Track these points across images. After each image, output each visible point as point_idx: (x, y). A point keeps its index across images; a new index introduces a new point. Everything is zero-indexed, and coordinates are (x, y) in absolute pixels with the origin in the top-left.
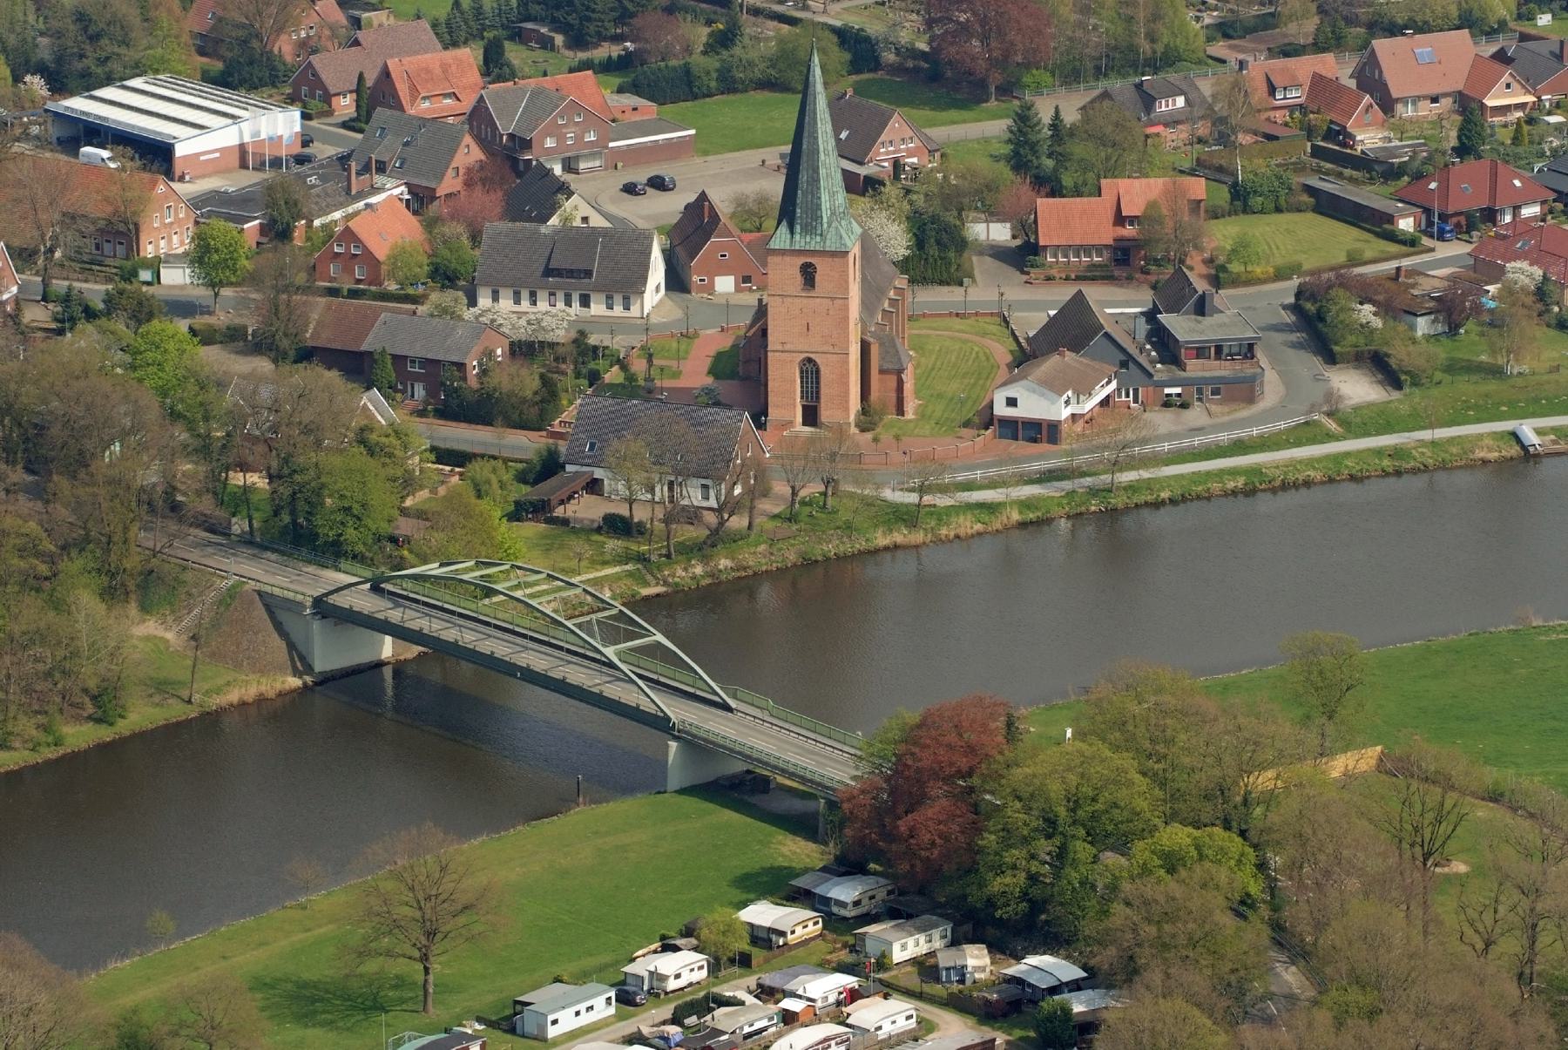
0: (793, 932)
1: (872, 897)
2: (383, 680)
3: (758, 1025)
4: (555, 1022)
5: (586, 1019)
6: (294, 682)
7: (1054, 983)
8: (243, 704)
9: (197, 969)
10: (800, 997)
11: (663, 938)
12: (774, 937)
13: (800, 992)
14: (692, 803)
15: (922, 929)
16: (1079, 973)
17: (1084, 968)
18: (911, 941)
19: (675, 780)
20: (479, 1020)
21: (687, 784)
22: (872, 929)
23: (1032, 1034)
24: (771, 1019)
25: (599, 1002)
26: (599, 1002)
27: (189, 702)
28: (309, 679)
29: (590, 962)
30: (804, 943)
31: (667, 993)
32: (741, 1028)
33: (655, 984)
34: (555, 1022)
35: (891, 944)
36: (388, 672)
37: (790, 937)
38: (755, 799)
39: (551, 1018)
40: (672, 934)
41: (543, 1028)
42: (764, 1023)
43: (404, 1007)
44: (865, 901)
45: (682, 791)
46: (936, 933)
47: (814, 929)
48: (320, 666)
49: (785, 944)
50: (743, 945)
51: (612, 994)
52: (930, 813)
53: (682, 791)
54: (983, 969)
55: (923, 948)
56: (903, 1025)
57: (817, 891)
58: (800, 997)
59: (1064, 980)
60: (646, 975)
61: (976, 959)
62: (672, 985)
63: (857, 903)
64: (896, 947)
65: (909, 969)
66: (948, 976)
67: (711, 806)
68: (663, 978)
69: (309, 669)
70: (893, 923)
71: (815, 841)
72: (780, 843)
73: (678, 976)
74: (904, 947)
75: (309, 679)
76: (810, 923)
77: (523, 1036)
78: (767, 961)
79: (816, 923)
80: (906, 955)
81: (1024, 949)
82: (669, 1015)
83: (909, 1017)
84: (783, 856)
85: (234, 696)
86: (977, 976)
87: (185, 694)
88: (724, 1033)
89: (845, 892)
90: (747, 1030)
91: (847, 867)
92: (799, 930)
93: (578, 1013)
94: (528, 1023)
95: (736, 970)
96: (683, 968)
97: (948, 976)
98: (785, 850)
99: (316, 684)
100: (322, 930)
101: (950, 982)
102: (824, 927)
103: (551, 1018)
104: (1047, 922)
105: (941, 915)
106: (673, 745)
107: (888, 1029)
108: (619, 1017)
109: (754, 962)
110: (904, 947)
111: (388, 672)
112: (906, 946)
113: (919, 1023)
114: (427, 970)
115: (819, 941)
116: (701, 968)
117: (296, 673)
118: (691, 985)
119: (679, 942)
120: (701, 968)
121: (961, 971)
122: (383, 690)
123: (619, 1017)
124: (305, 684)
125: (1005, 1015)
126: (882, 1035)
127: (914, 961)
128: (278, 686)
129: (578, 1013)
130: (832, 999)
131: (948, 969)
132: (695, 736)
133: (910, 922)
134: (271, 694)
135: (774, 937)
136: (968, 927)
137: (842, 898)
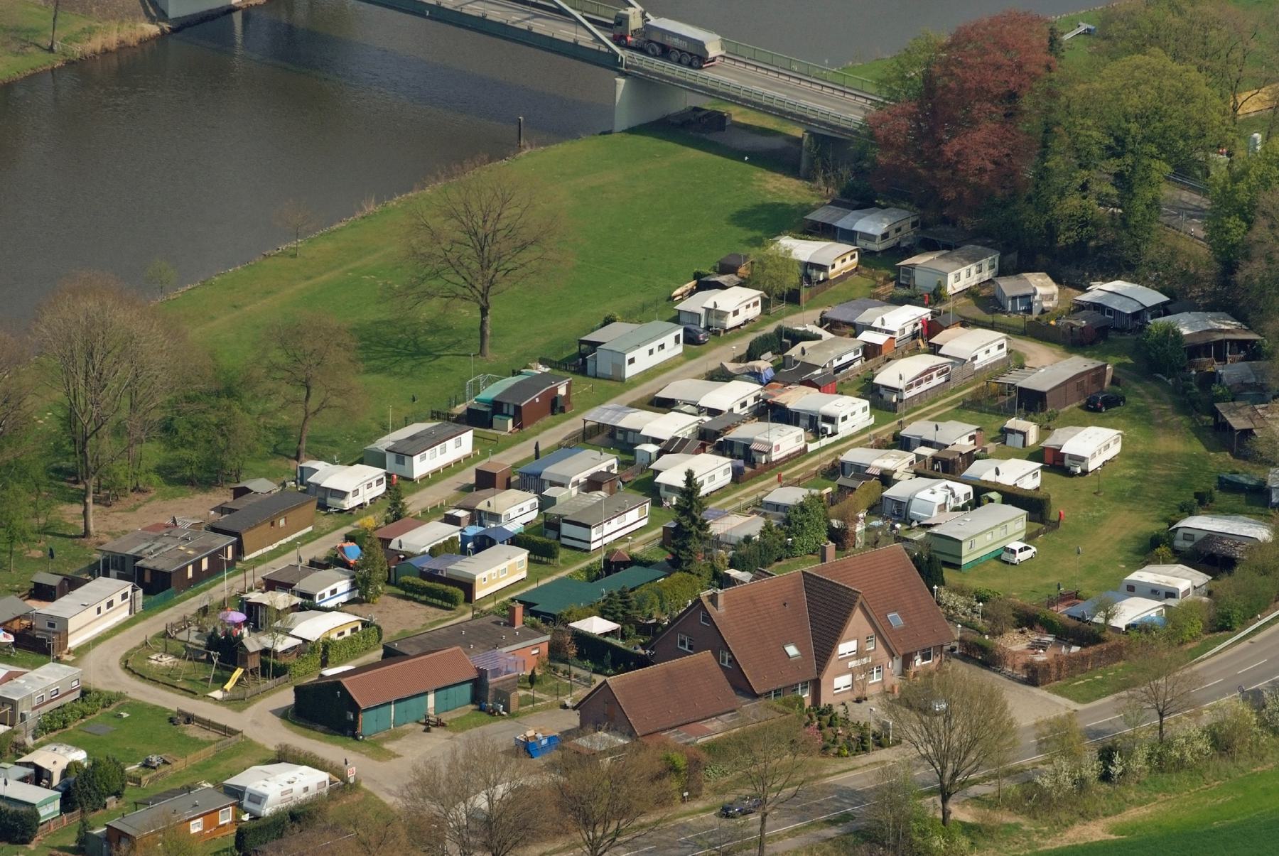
0: (833, 266)
1: (898, 230)
2: (232, 24)
3: (845, 359)
4: (632, 361)
5: (659, 357)
6: (153, 29)
7: (1136, 308)
8: (106, 52)
9: (212, 318)
10: (880, 330)
11: (697, 276)
12: (814, 273)
13: (877, 324)
14: (646, 143)
15: (973, 259)
16: (1158, 298)
17: (1162, 291)
18: (963, 271)
19: (623, 119)
20: (543, 362)
21: (635, 122)
22: (919, 260)
23: (1129, 360)
24: (857, 352)
25: (669, 340)
26: (669, 340)
27: (51, 50)
28: (166, 26)
29: (639, 299)
30: (843, 278)
31: (726, 331)
32: (831, 362)
33: (713, 322)
34: (632, 361)
35: (946, 275)
36: (237, 18)
37: (831, 271)
38: (714, 137)
39: (628, 357)
40: (706, 271)
41: (620, 368)
42: (850, 357)
43: (452, 351)
44: (892, 234)
45: (632, 131)
46: (985, 263)
47: (851, 263)
48: (173, 13)
49: (825, 280)
50: (793, 280)
51: (680, 332)
52: (978, 136)
53: (632, 131)
54: (1051, 297)
55: (974, 280)
56: (997, 354)
57: (839, 224)
58: (880, 330)
59: (1148, 305)
60: (702, 312)
61: (1043, 288)
62: (731, 322)
63: (885, 236)
64: (951, 278)
65: (963, 300)
66: (1014, 305)
67: (671, 145)
68: (723, 315)
69: (162, 15)
70: (937, 254)
71: (798, 177)
72: (760, 180)
73: (736, 313)
74: (958, 278)
75: (166, 26)
76: (848, 257)
77: (596, 377)
78: (812, 296)
79: (853, 257)
80: (960, 286)
81: (1090, 276)
82: (743, 351)
83: (1001, 346)
84: (770, 192)
85: (96, 44)
86: (1045, 304)
87: (46, 42)
88: (817, 367)
89: (873, 225)
90: (836, 364)
91: (861, 200)
92: (839, 265)
93: (651, 352)
94: (602, 363)
95: (784, 307)
96: (737, 303)
97: (1014, 305)
98: (769, 186)
99: (174, 31)
100: (325, 277)
101: (1015, 311)
102: (859, 262)
103: (628, 357)
104: (1098, 248)
105: (985, 245)
106: (621, 82)
107: (983, 360)
108: (687, 356)
109: (803, 297)
110: (958, 278)
111: (237, 18)
112: (961, 277)
113: (1009, 352)
114: (484, 311)
115: (855, 276)
116: (756, 304)
117: (152, 20)
118: (746, 322)
119: (722, 279)
120: (756, 304)
121: (1027, 299)
122: (233, 37)
123: (687, 356)
124: (162, 30)
125: (1092, 343)
126: (978, 364)
127: (969, 292)
128: (139, 34)
129: (651, 352)
130: (908, 332)
131: (1014, 298)
132: (648, 72)
133: (956, 253)
134: (132, 41)
135: (814, 273)
136: (1013, 257)
137: (870, 231)
